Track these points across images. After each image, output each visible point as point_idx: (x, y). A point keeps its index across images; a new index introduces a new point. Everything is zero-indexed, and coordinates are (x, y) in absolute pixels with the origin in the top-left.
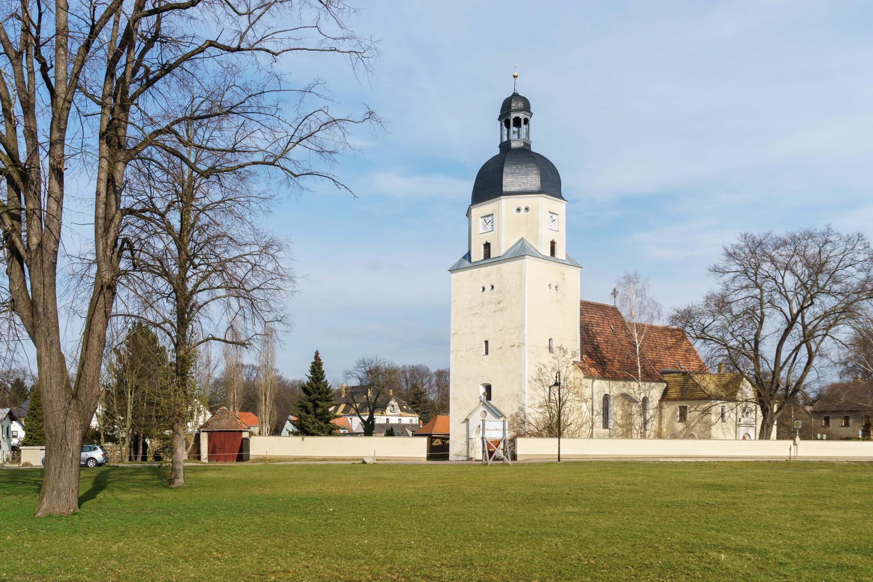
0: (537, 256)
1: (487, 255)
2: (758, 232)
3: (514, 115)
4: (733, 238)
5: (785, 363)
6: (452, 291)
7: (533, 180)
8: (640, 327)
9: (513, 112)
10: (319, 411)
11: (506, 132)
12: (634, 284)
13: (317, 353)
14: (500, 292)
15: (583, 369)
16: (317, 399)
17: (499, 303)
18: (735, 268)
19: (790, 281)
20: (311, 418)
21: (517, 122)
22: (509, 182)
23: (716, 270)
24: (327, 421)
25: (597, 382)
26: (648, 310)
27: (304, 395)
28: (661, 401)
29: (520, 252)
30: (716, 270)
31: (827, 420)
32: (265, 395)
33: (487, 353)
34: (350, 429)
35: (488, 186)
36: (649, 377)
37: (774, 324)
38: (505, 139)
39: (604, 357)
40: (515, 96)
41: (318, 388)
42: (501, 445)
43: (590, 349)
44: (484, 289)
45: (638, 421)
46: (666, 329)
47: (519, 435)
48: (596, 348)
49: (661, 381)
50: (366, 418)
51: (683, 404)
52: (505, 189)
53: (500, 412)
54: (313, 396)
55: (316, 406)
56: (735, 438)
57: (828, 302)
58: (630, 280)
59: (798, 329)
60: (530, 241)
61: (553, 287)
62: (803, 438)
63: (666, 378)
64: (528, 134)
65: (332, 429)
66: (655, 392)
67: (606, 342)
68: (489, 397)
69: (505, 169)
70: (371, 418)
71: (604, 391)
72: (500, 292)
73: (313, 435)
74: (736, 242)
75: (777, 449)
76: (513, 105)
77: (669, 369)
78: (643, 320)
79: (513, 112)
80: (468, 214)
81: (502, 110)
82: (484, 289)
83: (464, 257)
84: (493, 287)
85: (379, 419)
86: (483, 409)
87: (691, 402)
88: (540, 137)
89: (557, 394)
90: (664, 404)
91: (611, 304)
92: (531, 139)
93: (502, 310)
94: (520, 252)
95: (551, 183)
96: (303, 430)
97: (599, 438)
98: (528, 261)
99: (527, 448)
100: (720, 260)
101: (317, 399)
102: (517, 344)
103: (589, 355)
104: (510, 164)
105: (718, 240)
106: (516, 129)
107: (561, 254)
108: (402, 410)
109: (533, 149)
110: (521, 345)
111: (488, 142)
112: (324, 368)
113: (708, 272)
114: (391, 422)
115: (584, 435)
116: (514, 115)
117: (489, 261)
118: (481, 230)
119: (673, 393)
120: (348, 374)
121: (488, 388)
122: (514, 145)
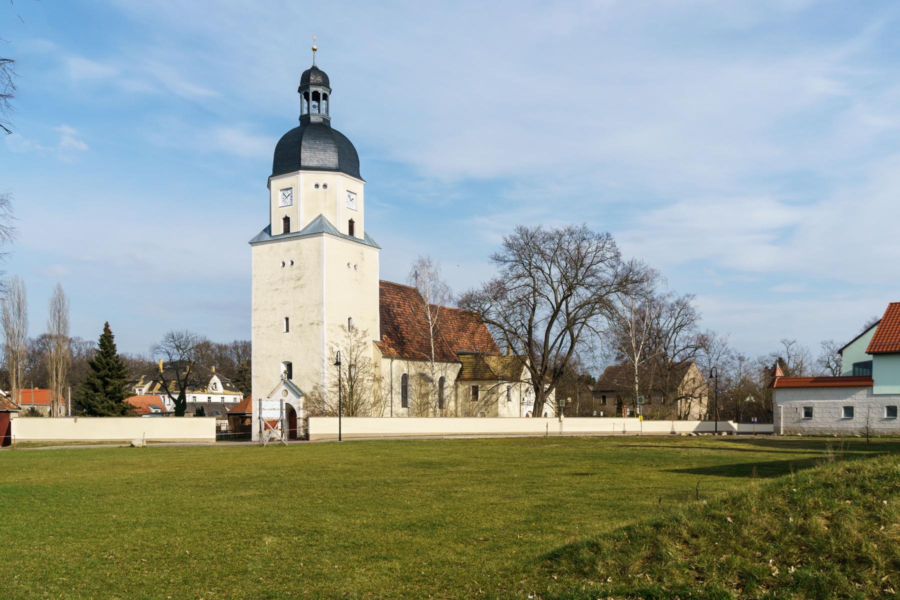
0: (336, 234)
1: (287, 229)
2: (531, 227)
3: (312, 89)
4: (511, 232)
5: (552, 347)
6: (253, 266)
7: (331, 158)
8: (433, 307)
9: (313, 85)
10: (110, 389)
11: (306, 105)
12: (428, 267)
13: (107, 325)
14: (299, 268)
15: (381, 348)
16: (107, 376)
17: (299, 279)
18: (512, 258)
19: (555, 273)
20: (100, 396)
21: (316, 96)
22: (307, 156)
23: (497, 259)
24: (120, 400)
25: (396, 362)
26: (441, 293)
27: (92, 372)
28: (456, 380)
29: (319, 228)
30: (497, 259)
31: (604, 398)
32: (57, 371)
33: (287, 331)
34: (163, 408)
35: (287, 159)
36: (444, 357)
37: (543, 312)
38: (305, 112)
39: (404, 338)
40: (314, 69)
41: (108, 364)
42: (279, 424)
43: (390, 330)
44: (284, 264)
45: (433, 399)
46: (455, 311)
47: (314, 414)
48: (396, 328)
49: (456, 361)
50: (176, 397)
51: (474, 384)
52: (303, 163)
53: (301, 391)
54: (102, 373)
55: (106, 384)
56: (515, 414)
57: (583, 294)
58: (424, 264)
59: (562, 317)
60: (329, 217)
61: (352, 266)
62: (567, 416)
63: (462, 358)
64: (327, 111)
65: (125, 409)
66: (451, 372)
67: (407, 323)
68: (290, 376)
69: (303, 143)
70: (182, 396)
71: (403, 370)
72: (299, 268)
73: (102, 415)
74: (514, 233)
75: (551, 424)
76: (312, 78)
77: (465, 350)
78: (438, 302)
79: (313, 85)
80: (269, 186)
81: (302, 82)
82: (284, 264)
83: (265, 230)
84: (292, 263)
85: (194, 397)
86: (284, 387)
87: (482, 382)
88: (341, 114)
89: (347, 373)
90: (459, 383)
91: (413, 286)
92: (330, 115)
93: (302, 286)
94: (319, 228)
95: (348, 162)
96: (85, 408)
97: (398, 417)
98: (326, 238)
99: (321, 428)
100: (502, 252)
101: (107, 376)
102: (316, 322)
103: (389, 335)
104: (309, 140)
105: (497, 231)
106: (315, 103)
107: (359, 233)
108: (225, 388)
109: (333, 126)
110: (320, 323)
111: (290, 110)
112: (115, 341)
113: (490, 260)
114: (213, 401)
115: (431, 414)
116: (312, 89)
117: (288, 236)
118: (281, 204)
119: (467, 374)
120: (156, 349)
121: (289, 366)
122: (313, 119)
